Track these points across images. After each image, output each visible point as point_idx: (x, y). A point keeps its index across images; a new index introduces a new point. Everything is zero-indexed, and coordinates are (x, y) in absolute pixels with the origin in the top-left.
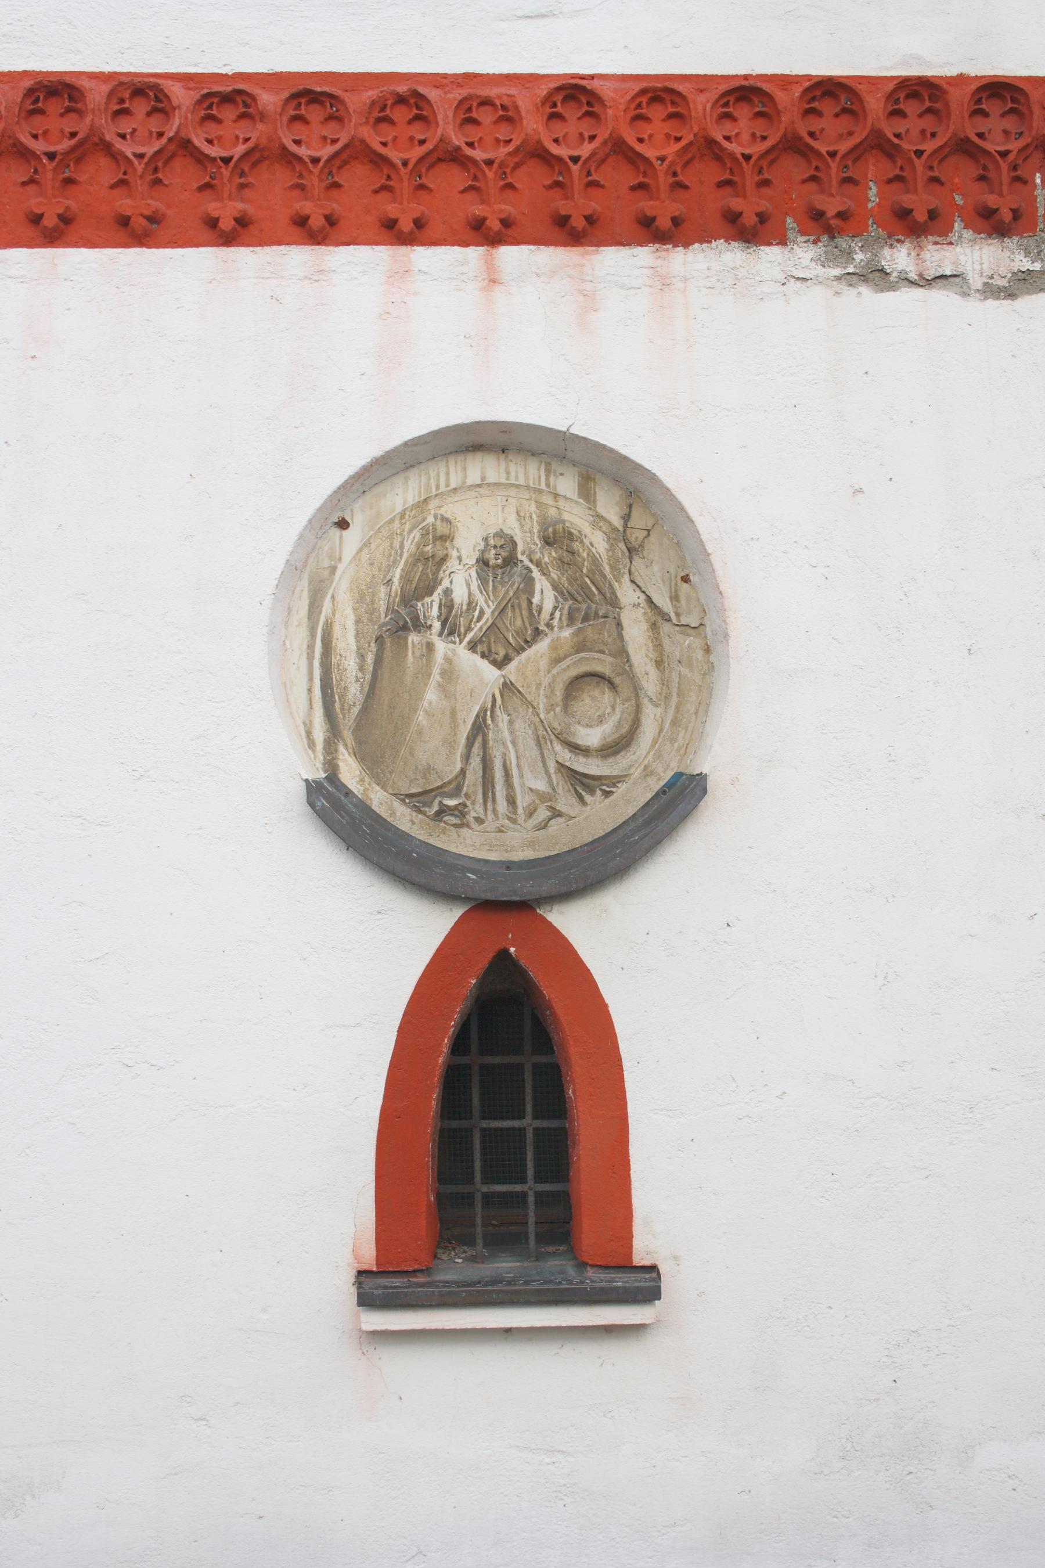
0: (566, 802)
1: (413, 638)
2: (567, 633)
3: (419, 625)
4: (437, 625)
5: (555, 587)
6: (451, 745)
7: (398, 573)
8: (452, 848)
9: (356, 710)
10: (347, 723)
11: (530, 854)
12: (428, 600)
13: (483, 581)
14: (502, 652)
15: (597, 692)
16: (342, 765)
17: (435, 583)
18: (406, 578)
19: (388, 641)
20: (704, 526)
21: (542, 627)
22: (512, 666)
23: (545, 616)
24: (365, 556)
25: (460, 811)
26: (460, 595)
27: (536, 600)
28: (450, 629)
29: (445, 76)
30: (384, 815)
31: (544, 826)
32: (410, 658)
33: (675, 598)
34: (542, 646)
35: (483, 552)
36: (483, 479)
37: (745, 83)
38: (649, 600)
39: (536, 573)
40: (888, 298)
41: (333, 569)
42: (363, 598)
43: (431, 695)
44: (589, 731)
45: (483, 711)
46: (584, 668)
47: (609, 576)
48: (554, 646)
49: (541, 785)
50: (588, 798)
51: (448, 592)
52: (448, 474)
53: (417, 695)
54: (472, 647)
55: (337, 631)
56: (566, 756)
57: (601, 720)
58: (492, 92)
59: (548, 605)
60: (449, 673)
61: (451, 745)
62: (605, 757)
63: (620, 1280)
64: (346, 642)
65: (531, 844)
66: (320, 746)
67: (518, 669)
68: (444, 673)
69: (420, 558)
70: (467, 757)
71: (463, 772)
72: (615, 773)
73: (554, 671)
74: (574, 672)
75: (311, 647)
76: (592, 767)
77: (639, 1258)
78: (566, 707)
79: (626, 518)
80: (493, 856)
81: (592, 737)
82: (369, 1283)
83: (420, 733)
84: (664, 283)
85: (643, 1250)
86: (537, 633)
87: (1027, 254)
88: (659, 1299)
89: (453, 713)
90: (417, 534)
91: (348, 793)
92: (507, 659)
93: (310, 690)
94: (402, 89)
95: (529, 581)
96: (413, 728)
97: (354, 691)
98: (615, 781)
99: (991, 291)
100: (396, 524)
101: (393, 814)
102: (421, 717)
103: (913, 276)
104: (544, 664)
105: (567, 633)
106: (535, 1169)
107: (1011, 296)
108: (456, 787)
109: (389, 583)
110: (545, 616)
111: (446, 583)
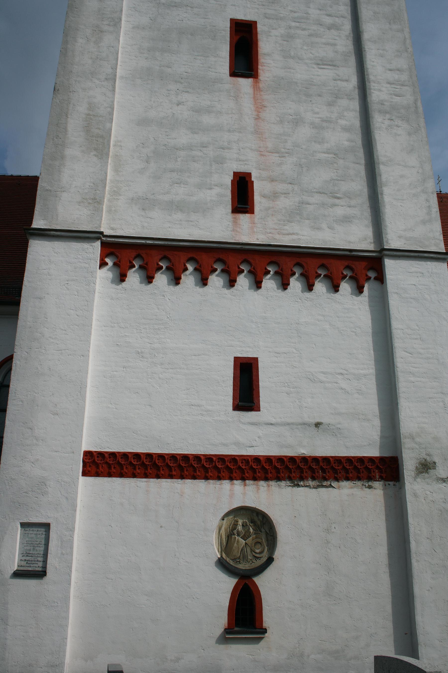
0: (254, 561)
1: (233, 536)
2: (254, 536)
3: (234, 534)
4: (236, 534)
5: (253, 529)
6: (238, 552)
7: (231, 527)
8: (238, 567)
9: (225, 546)
10: (223, 548)
11: (249, 568)
12: (235, 531)
13: (243, 528)
14: (245, 539)
15: (258, 545)
16: (223, 555)
17: (236, 528)
18: (232, 527)
19: (230, 537)
20: (274, 522)
21: (251, 535)
22: (247, 541)
23: (251, 533)
24: (226, 524)
25: (239, 562)
26: (240, 530)
27: (250, 531)
28: (238, 535)
29: (239, 455)
30: (229, 562)
31: (251, 564)
32: (233, 539)
33: (269, 531)
34: (251, 538)
35: (243, 524)
36: (243, 513)
37: (280, 457)
38: (266, 531)
39: (250, 527)
40: (300, 488)
41: (222, 526)
42: (226, 530)
43: (235, 545)
44: (257, 550)
45: (242, 548)
46: (257, 541)
47: (260, 527)
48: (253, 538)
49: (250, 558)
50: (257, 560)
51: (238, 529)
52: (238, 512)
53: (233, 545)
54: (241, 538)
55: (222, 535)
56: (254, 554)
57: (259, 549)
58: (245, 458)
59: (252, 531)
60: (238, 541)
61: (238, 552)
62: (260, 554)
63: (261, 630)
64: (224, 537)
65: (249, 567)
66: (220, 552)
67: (248, 541)
68: (237, 541)
69: (234, 524)
70: (240, 554)
71: (240, 556)
72: (261, 556)
73: (253, 541)
74: (255, 542)
75: (219, 537)
76: (258, 555)
77: (264, 627)
78: (254, 546)
79: (263, 519)
80: (244, 568)
81: (258, 551)
82: (227, 630)
83: (234, 550)
84: (268, 486)
85: (265, 625)
86: (251, 536)
87: (319, 482)
88: (267, 633)
89: (238, 547)
90: (234, 521)
91: (224, 559)
92: (246, 539)
93: (219, 544)
94: (233, 457)
95: (249, 528)
96: (233, 549)
97: (225, 544)
98: (261, 557)
99: (314, 488)
100: (231, 519)
101: (230, 562)
102: (234, 548)
103: (303, 485)
104: (251, 540)
105: (254, 536)
106: (272, 479)
107: (317, 488)
108: (239, 558)
109: (230, 528)
110: (251, 533)
111: (238, 528)
